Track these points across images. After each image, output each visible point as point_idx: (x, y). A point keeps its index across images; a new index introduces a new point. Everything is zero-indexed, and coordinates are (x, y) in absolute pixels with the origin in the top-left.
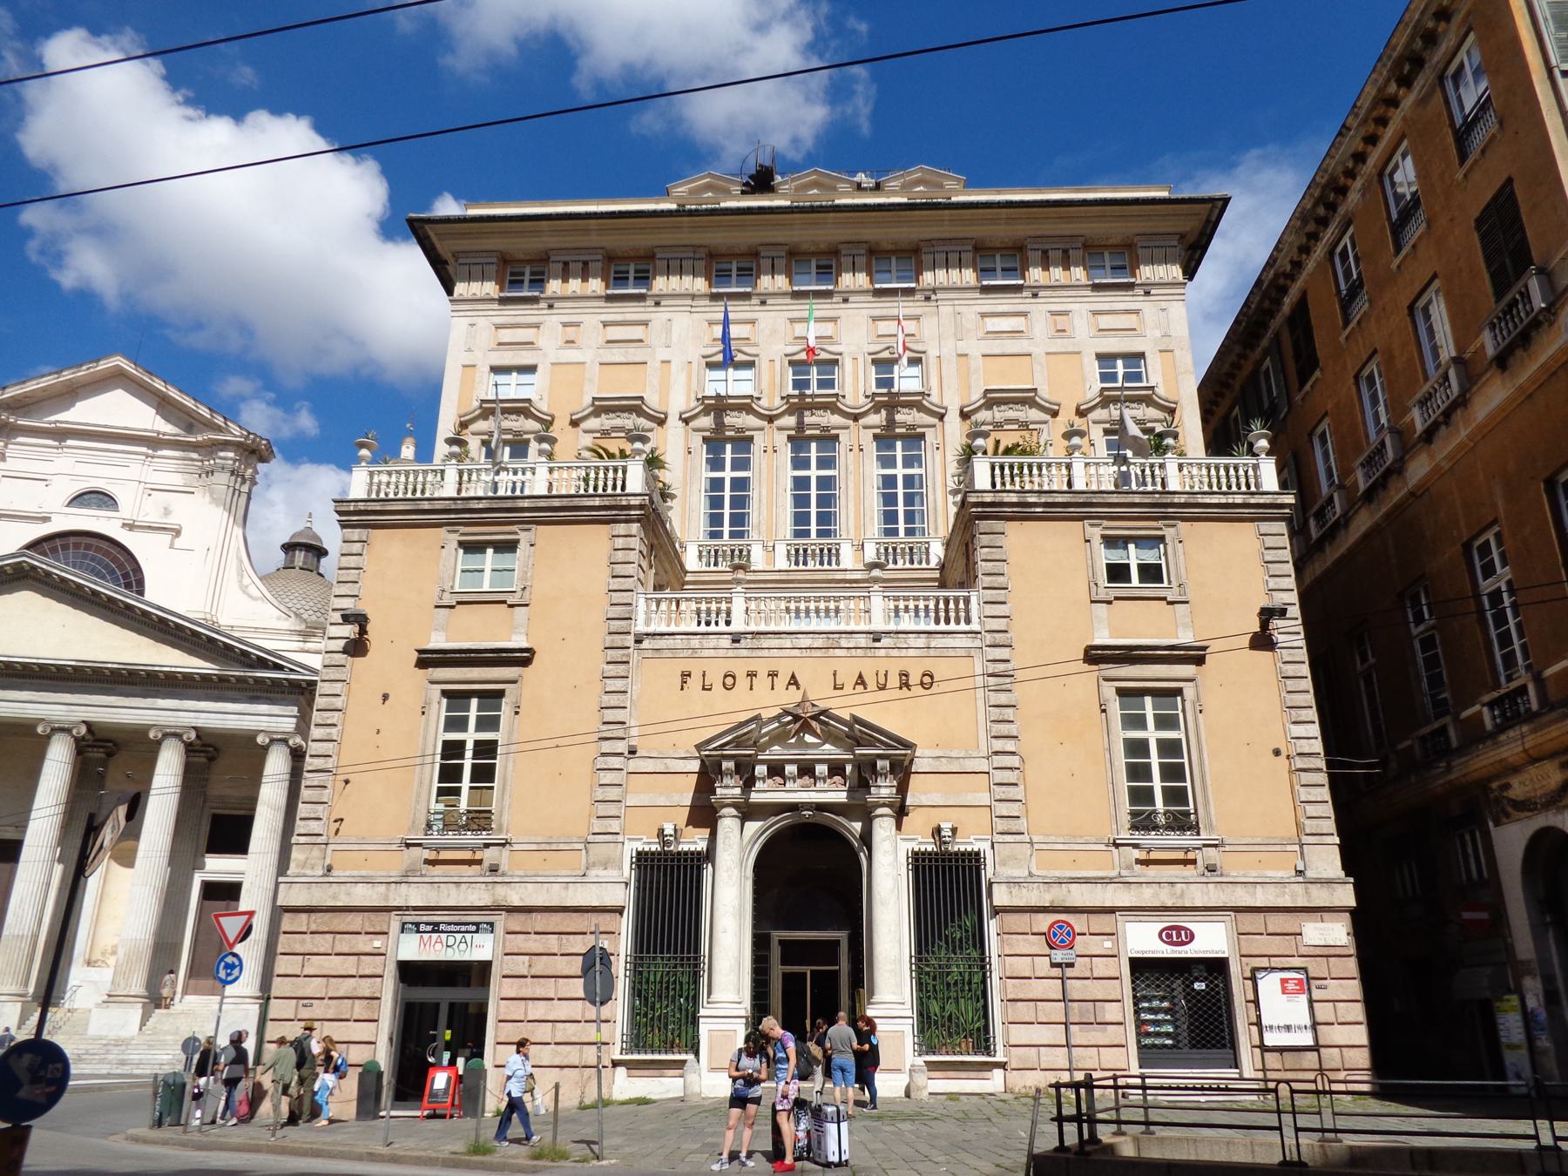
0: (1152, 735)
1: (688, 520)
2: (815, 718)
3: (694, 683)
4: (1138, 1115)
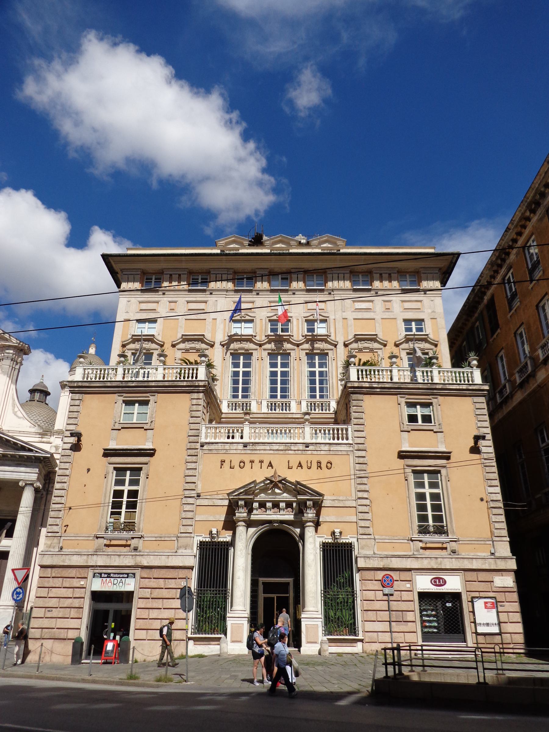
0: (427, 491)
1: (223, 391)
2: (280, 482)
3: (227, 465)
4: (420, 662)
